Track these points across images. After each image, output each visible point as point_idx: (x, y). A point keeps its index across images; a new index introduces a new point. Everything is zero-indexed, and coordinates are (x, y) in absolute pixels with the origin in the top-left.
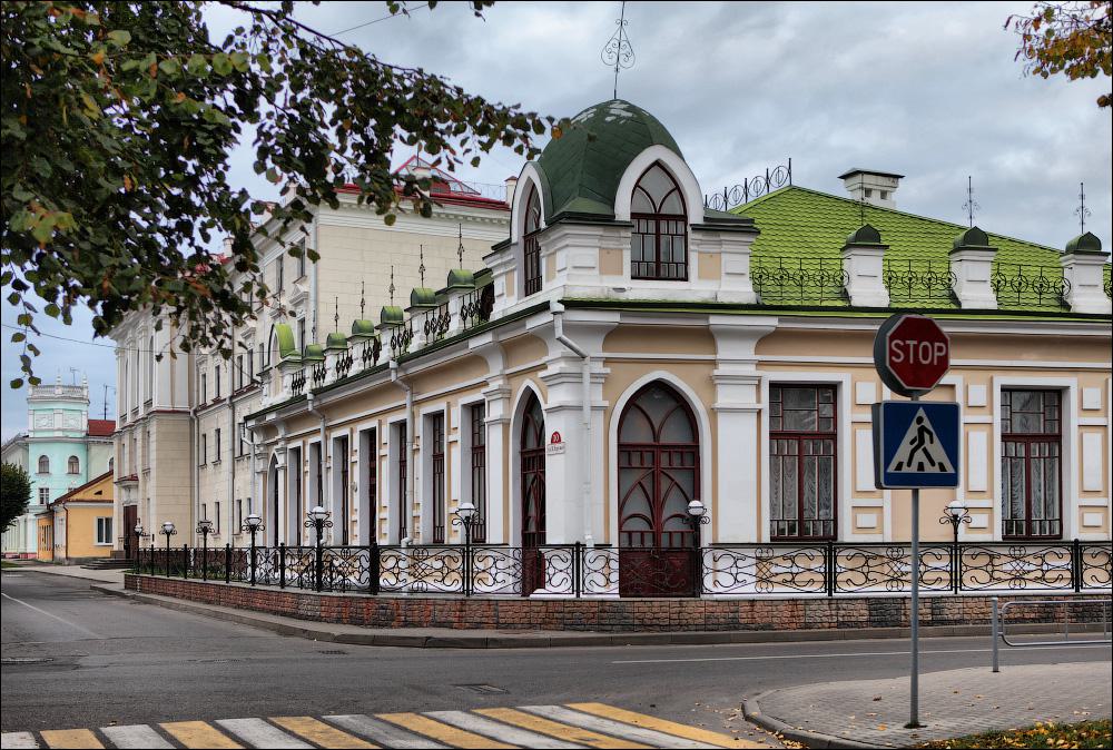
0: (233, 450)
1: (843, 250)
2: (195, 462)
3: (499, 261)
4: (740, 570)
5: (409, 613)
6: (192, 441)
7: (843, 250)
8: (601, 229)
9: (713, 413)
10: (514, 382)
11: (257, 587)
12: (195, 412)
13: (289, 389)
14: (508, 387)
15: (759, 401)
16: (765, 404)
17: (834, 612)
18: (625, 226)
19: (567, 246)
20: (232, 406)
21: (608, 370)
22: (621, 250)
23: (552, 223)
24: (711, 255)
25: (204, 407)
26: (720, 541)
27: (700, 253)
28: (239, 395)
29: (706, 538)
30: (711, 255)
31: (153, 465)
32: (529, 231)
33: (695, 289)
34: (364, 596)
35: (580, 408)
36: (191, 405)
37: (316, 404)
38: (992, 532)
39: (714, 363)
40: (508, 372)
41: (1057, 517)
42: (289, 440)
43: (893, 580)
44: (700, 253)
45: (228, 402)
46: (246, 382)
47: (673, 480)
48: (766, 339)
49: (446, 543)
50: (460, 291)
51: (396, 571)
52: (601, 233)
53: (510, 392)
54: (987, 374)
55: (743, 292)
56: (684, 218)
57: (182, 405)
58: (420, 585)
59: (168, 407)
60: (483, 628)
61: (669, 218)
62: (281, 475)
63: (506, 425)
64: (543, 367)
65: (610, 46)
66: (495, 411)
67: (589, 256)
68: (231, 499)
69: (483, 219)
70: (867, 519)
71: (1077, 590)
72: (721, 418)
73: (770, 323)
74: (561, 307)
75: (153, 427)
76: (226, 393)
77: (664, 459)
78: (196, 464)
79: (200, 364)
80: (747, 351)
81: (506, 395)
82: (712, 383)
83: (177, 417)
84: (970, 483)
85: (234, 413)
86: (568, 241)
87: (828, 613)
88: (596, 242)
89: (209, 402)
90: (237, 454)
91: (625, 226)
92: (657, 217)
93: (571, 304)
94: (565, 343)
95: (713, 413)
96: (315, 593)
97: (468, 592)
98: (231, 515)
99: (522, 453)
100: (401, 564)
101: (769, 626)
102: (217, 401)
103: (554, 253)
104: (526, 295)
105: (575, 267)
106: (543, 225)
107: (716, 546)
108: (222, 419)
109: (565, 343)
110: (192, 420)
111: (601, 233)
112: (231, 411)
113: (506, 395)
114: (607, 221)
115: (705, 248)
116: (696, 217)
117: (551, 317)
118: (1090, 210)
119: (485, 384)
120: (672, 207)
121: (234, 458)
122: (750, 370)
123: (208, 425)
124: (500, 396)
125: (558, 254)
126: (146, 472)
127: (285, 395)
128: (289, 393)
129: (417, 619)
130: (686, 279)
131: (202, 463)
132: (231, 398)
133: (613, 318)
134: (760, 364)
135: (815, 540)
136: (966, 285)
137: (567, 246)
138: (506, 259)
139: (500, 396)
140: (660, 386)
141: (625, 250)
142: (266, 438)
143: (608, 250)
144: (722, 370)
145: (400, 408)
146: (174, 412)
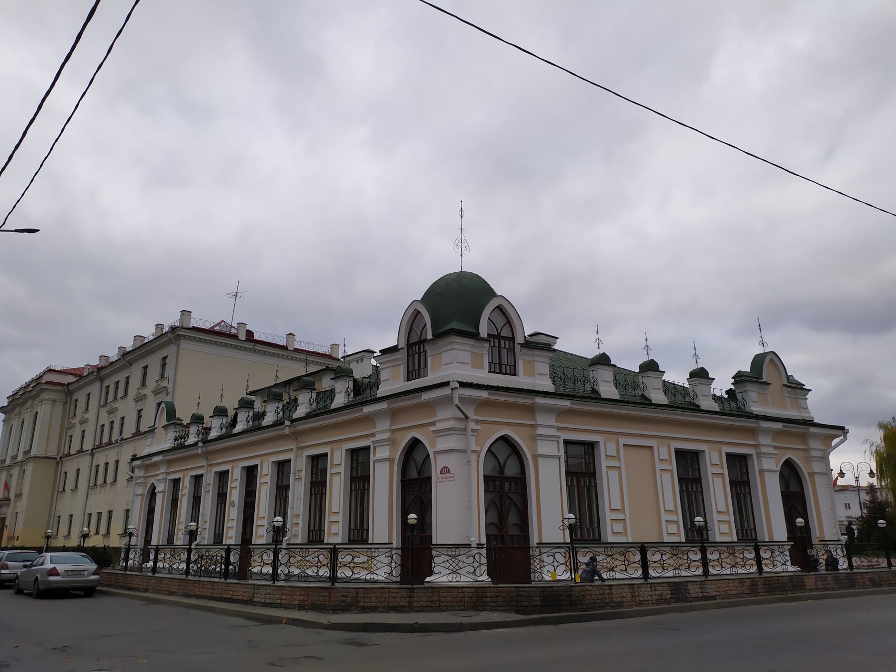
0: (89, 481)
1: (589, 366)
2: (58, 490)
3: (389, 359)
4: (623, 563)
5: (367, 600)
6: (55, 476)
7: (589, 366)
8: (473, 340)
9: (536, 457)
10: (149, 479)
11: (128, 572)
12: (61, 458)
13: (172, 441)
14: (145, 481)
15: (559, 451)
16: (562, 453)
17: (654, 592)
18: (483, 340)
19: (454, 349)
20: (92, 455)
21: (777, 452)
22: (483, 354)
23: (438, 336)
24: (529, 362)
25: (69, 455)
26: (374, 542)
27: (524, 360)
28: (97, 448)
29: (534, 540)
30: (529, 362)
31: (26, 491)
32: (412, 341)
33: (521, 381)
34: (135, 573)
35: (464, 451)
36: (58, 453)
37: (204, 449)
38: (626, 535)
39: (534, 427)
40: (394, 427)
41: (596, 526)
42: (168, 474)
43: (676, 569)
44: (524, 360)
45: (89, 452)
46: (105, 440)
47: (512, 500)
48: (562, 413)
49: (325, 542)
50: (345, 378)
51: (352, 565)
52: (472, 343)
53: (394, 441)
54: (667, 441)
55: (547, 385)
56: (513, 339)
57: (52, 453)
58: (372, 576)
59: (42, 453)
60: (428, 611)
61: (506, 338)
62: (159, 498)
63: (391, 460)
64: (434, 423)
65: (457, 242)
66: (380, 453)
67: (466, 356)
68: (83, 513)
69: (274, 353)
70: (618, 527)
71: (333, 584)
72: (540, 460)
73: (566, 403)
74: (457, 385)
75: (29, 468)
76: (88, 446)
77: (507, 485)
78: (56, 490)
79: (69, 429)
80: (551, 420)
81: (392, 442)
82: (534, 438)
83: (48, 460)
84: (612, 506)
85: (92, 459)
86: (455, 346)
87: (650, 593)
88: (468, 348)
89: (73, 452)
90: (92, 484)
91: (483, 340)
92: (499, 337)
93: (463, 385)
94: (459, 408)
95: (536, 457)
96: (222, 580)
97: (333, 578)
98: (82, 523)
99: (402, 481)
100: (137, 556)
101: (621, 604)
102: (81, 451)
103: (441, 353)
104: (408, 381)
105: (458, 362)
106: (430, 336)
107: (541, 544)
108: (84, 463)
109: (459, 408)
110: (58, 463)
111: (472, 343)
112: (91, 457)
113: (392, 442)
114: (474, 336)
115: (526, 358)
116: (520, 339)
117: (450, 392)
118: (699, 356)
119: (373, 435)
120: (506, 333)
121: (89, 487)
122: (553, 432)
123: (70, 467)
124: (388, 443)
125: (443, 354)
126: (19, 496)
127: (168, 444)
128: (172, 443)
129: (374, 605)
130: (515, 375)
131: (61, 489)
132: (92, 450)
133: (779, 426)
134: (559, 429)
135: (582, 540)
136: (651, 390)
137: (454, 349)
138: (475, 344)
139: (388, 443)
140: (504, 439)
141: (484, 353)
142: (145, 473)
143: (475, 354)
144: (540, 431)
145: (285, 451)
146: (46, 458)
